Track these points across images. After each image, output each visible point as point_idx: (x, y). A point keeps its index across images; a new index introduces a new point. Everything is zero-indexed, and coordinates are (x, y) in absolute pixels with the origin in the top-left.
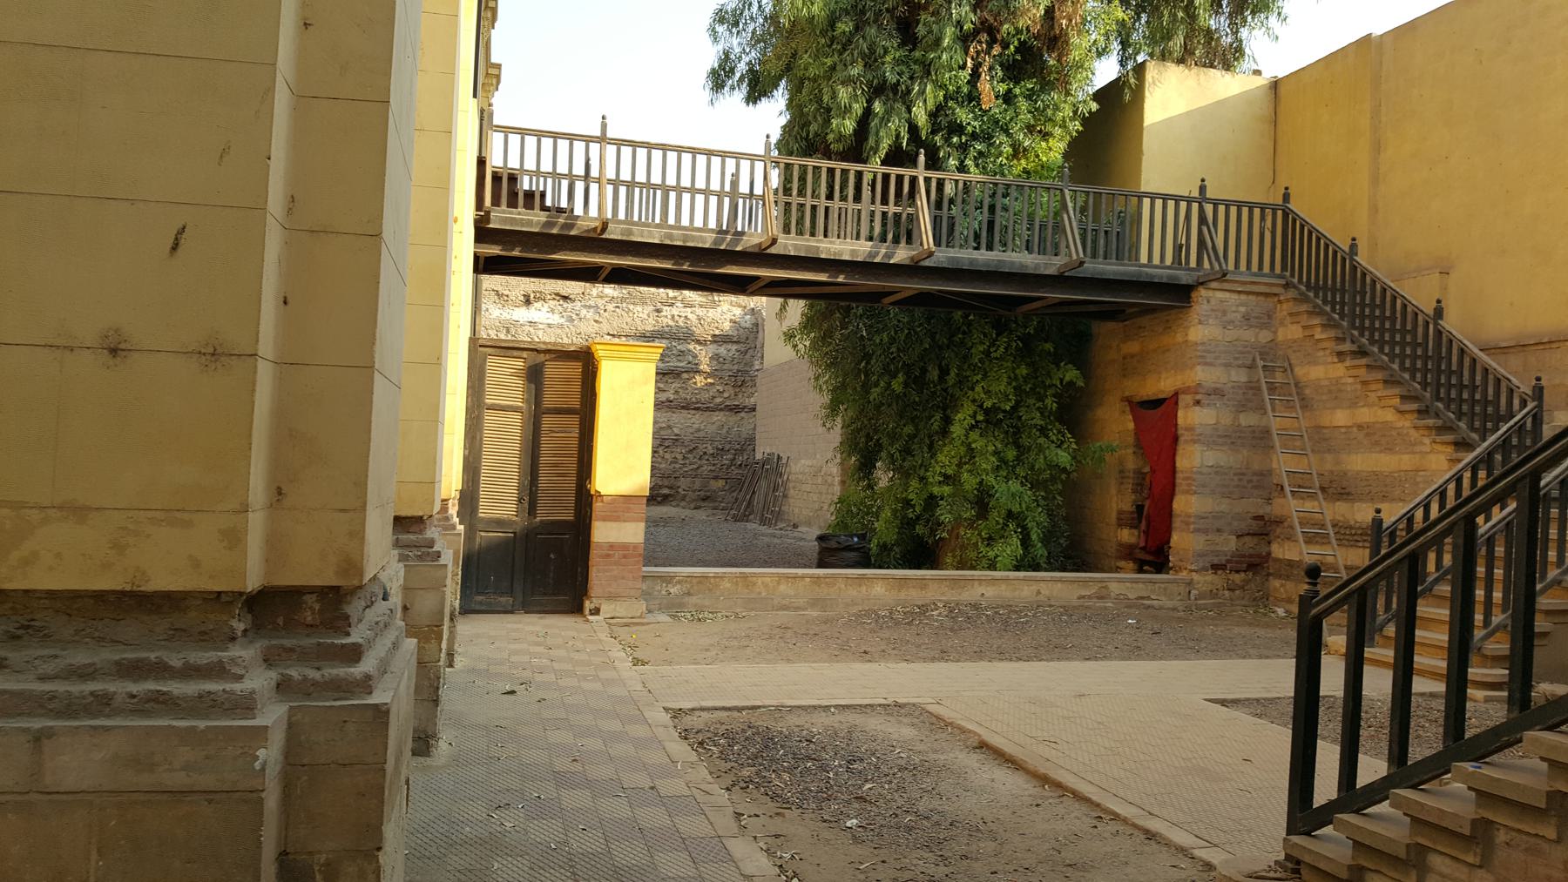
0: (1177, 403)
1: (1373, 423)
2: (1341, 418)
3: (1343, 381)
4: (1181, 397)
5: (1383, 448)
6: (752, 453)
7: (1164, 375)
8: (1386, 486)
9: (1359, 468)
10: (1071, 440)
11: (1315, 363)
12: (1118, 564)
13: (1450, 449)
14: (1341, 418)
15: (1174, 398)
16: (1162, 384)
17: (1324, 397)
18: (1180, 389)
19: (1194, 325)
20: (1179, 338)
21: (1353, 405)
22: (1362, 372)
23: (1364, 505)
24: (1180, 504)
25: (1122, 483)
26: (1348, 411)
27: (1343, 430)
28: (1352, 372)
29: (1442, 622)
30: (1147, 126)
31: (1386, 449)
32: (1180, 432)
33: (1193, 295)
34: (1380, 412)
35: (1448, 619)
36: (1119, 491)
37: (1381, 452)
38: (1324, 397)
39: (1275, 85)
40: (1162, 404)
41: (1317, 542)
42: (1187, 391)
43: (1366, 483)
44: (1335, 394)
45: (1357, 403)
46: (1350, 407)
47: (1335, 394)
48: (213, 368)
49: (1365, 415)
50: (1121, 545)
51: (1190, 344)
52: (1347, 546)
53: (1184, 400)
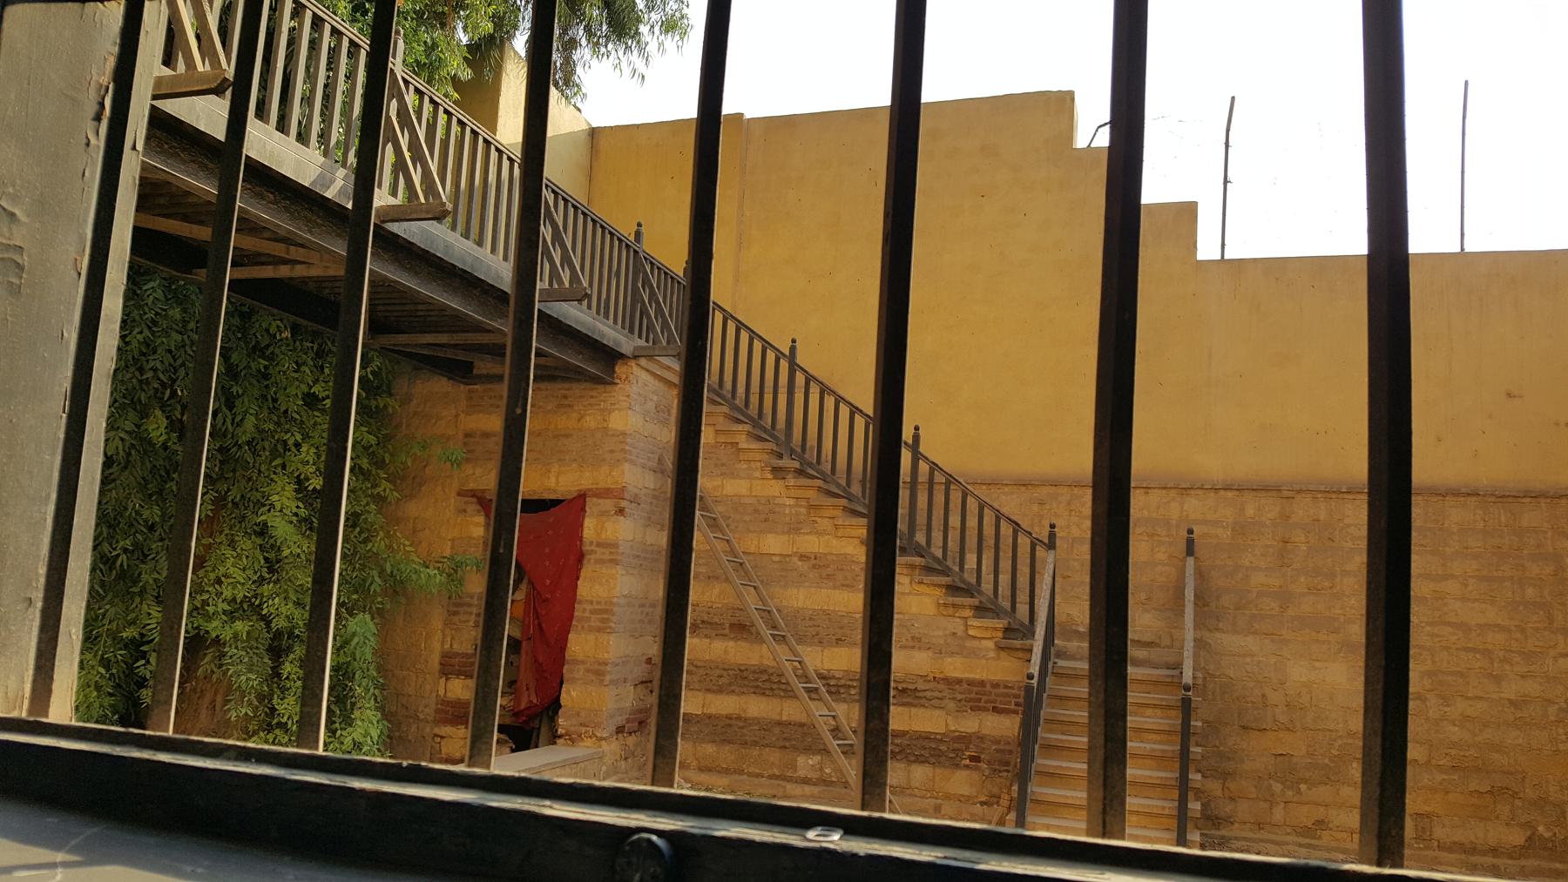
0: (583, 509)
1: (825, 554)
2: (774, 544)
3: (780, 501)
4: (590, 502)
5: (838, 584)
6: (990, 706)
7: (555, 468)
8: (842, 628)
9: (800, 605)
10: (408, 549)
11: (734, 475)
12: (437, 731)
13: (938, 592)
14: (774, 544)
15: (578, 503)
16: (553, 480)
17: (747, 518)
18: (589, 490)
19: (620, 410)
20: (590, 421)
21: (794, 529)
22: (811, 494)
23: (809, 649)
24: (579, 645)
25: (456, 613)
26: (785, 538)
27: (776, 559)
28: (793, 493)
29: (1079, 807)
30: (725, 115)
31: (843, 585)
32: (586, 548)
33: (620, 369)
34: (835, 542)
35: (1085, 803)
36: (447, 624)
37: (835, 588)
38: (747, 518)
39: (594, 133)
40: (559, 504)
41: (733, 691)
42: (605, 493)
43: (811, 623)
44: (766, 516)
45: (799, 529)
46: (789, 533)
47: (766, 516)
48: (391, 675)
49: (811, 543)
50: (445, 702)
51: (610, 433)
52: (781, 697)
53: (592, 505)
